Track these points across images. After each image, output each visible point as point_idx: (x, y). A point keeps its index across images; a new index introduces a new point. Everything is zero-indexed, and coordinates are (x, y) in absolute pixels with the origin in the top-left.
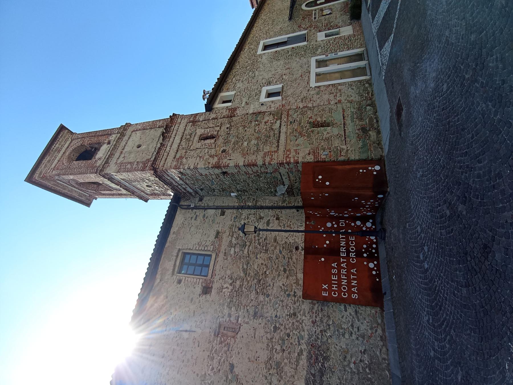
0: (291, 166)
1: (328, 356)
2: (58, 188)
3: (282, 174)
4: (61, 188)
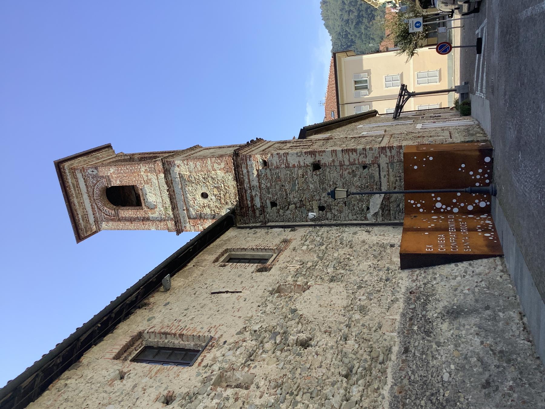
0: (394, 152)
1: (402, 36)
2: (73, 192)
3: (381, 167)
4: (75, 193)
